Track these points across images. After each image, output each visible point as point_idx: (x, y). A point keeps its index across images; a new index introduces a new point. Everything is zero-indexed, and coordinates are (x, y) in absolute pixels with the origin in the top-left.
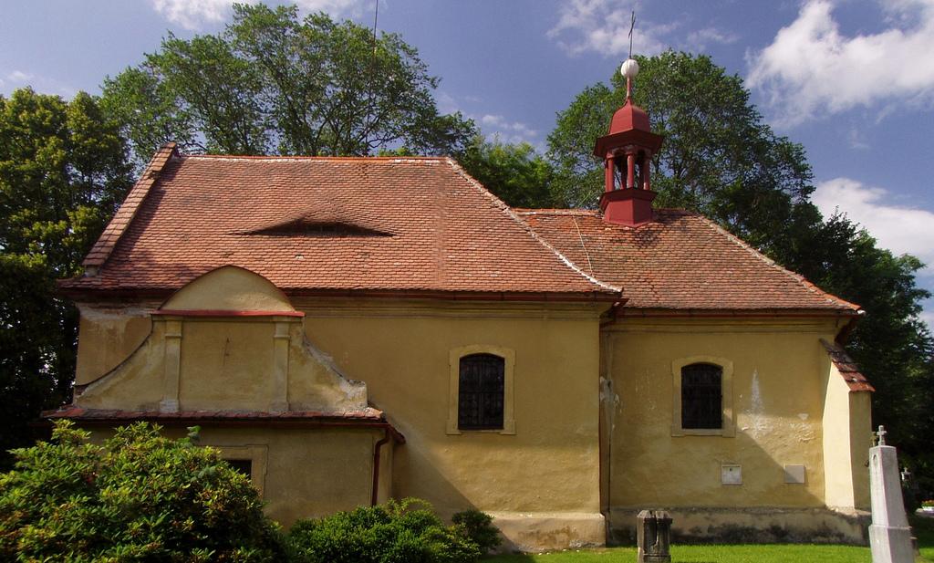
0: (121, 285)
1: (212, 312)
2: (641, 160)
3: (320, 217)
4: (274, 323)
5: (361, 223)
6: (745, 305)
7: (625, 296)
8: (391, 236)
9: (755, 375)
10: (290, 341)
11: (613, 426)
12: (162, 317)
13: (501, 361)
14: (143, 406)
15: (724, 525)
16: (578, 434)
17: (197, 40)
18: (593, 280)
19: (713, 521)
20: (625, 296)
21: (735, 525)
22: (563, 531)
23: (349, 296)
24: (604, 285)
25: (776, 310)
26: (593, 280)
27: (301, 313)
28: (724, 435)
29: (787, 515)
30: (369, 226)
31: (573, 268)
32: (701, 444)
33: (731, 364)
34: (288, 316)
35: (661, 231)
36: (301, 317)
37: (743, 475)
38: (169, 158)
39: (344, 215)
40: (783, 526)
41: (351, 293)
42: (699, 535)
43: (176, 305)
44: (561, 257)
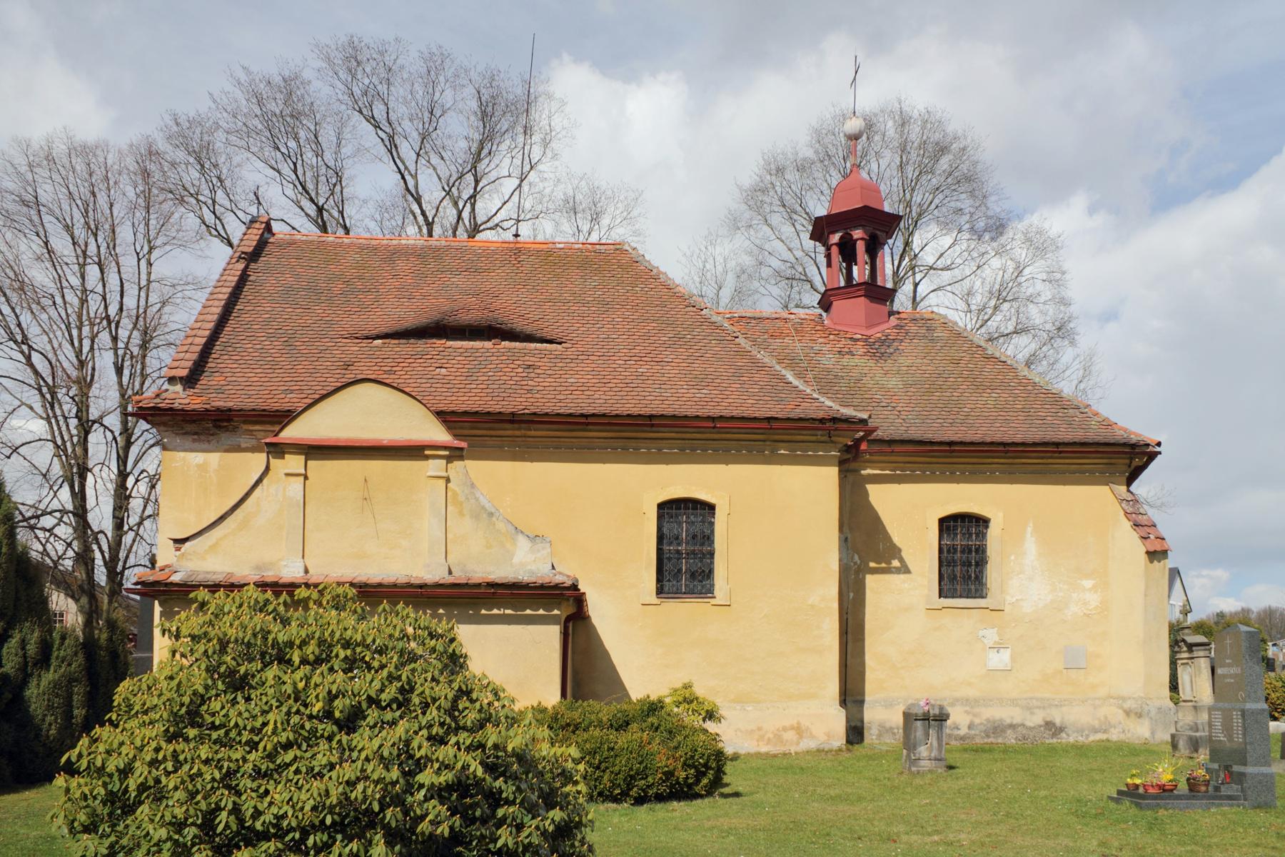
0: (213, 404)
1: (385, 443)
2: (874, 247)
3: (466, 318)
4: (427, 457)
5: (519, 325)
6: (977, 438)
7: (871, 424)
8: (560, 343)
9: (1029, 530)
10: (448, 480)
11: (851, 595)
12: (278, 450)
13: (711, 508)
14: (258, 568)
15: (988, 720)
16: (812, 606)
17: (131, 146)
18: (829, 403)
19: (975, 715)
20: (871, 424)
21: (1001, 720)
22: (792, 728)
23: (512, 422)
24: (836, 407)
25: (1057, 444)
26: (829, 403)
27: (463, 444)
28: (880, 591)
29: (1064, 709)
30: (529, 329)
31: (801, 387)
32: (962, 617)
33: (1001, 515)
34: (445, 448)
35: (902, 341)
36: (462, 449)
37: (1013, 659)
38: (262, 234)
39: (495, 315)
40: (1058, 722)
41: (514, 419)
42: (956, 732)
43: (294, 432)
44: (784, 372)
